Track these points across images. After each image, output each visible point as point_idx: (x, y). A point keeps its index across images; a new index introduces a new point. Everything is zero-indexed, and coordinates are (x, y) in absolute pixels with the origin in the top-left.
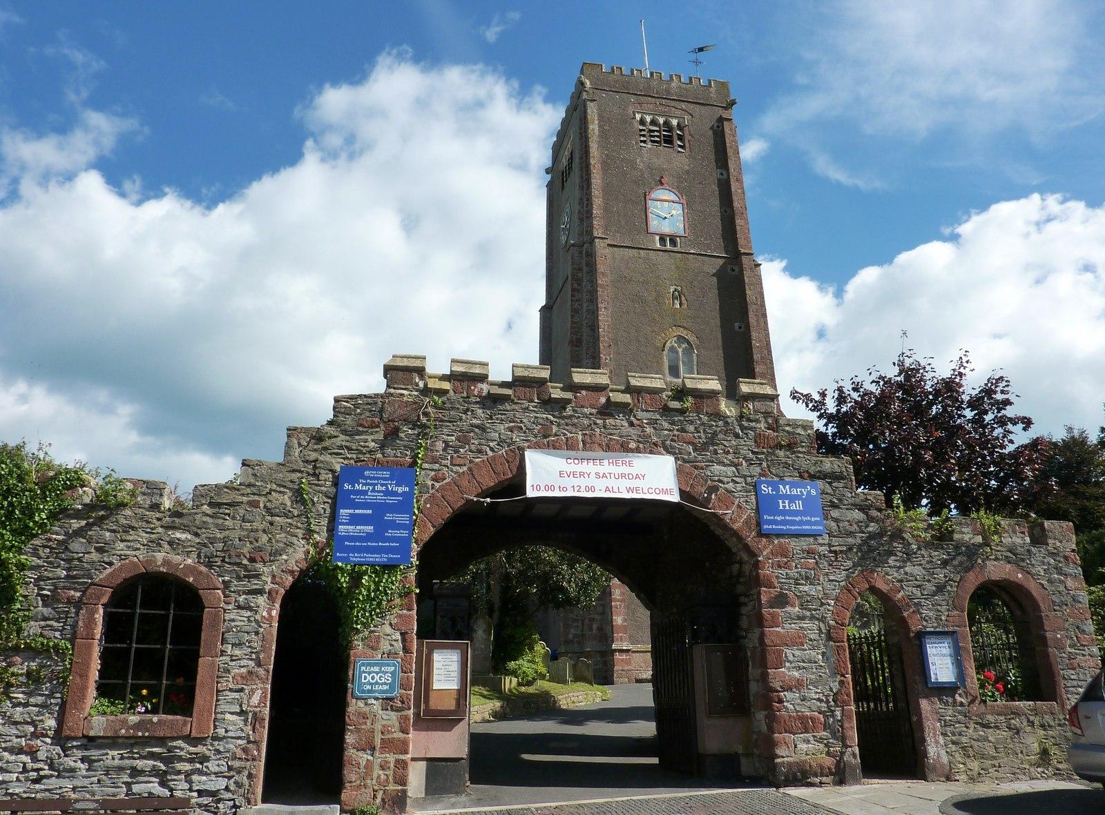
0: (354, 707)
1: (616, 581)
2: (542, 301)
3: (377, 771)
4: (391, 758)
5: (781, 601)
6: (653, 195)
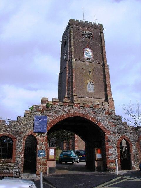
0: (38, 158)
1: (76, 135)
2: (59, 72)
3: (42, 169)
4: (44, 166)
5: (109, 141)
6: (85, 49)
